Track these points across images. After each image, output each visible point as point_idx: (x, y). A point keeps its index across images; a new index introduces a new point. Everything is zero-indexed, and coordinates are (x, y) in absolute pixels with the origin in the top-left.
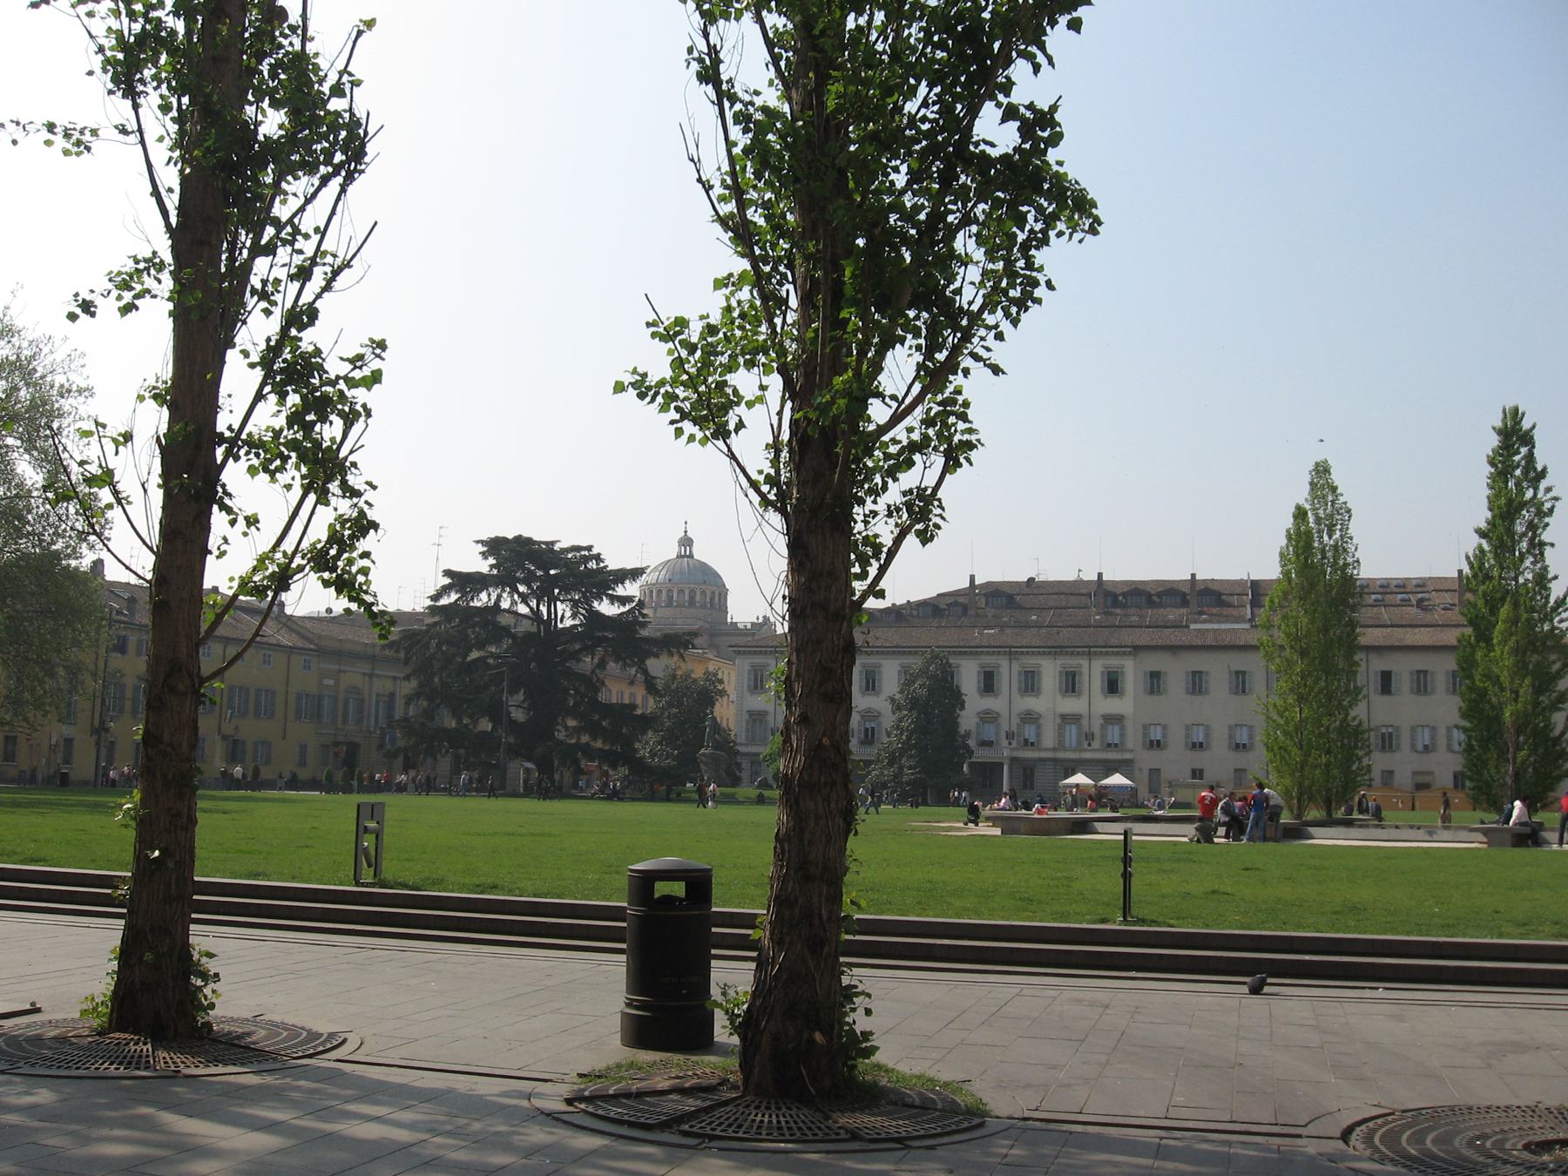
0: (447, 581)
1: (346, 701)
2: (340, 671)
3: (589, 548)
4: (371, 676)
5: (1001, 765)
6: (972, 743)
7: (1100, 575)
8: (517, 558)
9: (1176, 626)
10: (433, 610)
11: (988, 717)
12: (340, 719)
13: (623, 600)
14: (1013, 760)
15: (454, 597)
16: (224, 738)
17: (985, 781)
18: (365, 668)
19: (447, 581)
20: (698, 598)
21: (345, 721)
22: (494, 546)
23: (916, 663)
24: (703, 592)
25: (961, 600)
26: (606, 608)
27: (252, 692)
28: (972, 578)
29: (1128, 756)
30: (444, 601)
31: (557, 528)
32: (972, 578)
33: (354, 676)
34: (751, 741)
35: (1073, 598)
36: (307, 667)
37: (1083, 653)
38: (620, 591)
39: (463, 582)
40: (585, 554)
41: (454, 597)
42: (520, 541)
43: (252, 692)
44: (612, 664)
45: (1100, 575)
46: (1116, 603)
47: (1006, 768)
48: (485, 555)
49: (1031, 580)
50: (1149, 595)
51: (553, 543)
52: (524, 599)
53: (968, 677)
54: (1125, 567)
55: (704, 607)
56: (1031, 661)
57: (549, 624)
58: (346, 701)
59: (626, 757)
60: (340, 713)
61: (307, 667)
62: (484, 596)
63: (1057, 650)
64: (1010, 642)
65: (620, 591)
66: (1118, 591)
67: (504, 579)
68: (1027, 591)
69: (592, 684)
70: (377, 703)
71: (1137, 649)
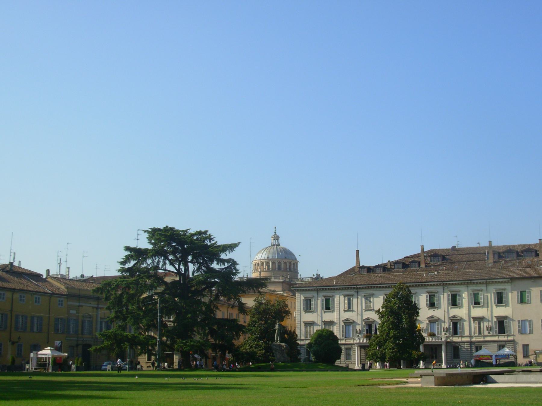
0: (127, 253)
1: (83, 322)
2: (79, 306)
3: (205, 232)
4: (97, 308)
5: (441, 345)
6: (424, 334)
7: (490, 242)
8: (169, 241)
9: (533, 266)
10: (122, 270)
11: (432, 320)
12: (80, 332)
13: (223, 261)
14: (447, 343)
15: (132, 263)
16: (13, 343)
17: (432, 354)
18: (94, 304)
19: (127, 253)
20: (282, 266)
21: (82, 333)
22: (155, 234)
23: (389, 291)
24: (285, 263)
25: (417, 259)
26: (215, 266)
27: (29, 319)
28: (422, 247)
29: (510, 338)
30: (127, 266)
31: (186, 223)
32: (422, 247)
33: (87, 308)
34: (346, 337)
35: (475, 256)
36: (61, 303)
37: (483, 283)
38: (223, 256)
39: (136, 253)
40: (203, 235)
41: (132, 263)
42: (166, 229)
43: (29, 319)
44: (222, 298)
45: (490, 242)
46: (500, 257)
47: (443, 346)
48: (150, 239)
49: (454, 247)
50: (517, 253)
51: (186, 231)
52: (172, 263)
53: (422, 300)
54: (503, 240)
55: (285, 270)
56: (455, 288)
57: (184, 276)
58: (83, 322)
59: (226, 346)
60: (80, 328)
61: (61, 303)
62: (149, 261)
63: (468, 282)
64: (443, 279)
65: (223, 256)
66: (501, 251)
67: (158, 252)
68: (452, 253)
69: (210, 309)
70: (101, 324)
71: (512, 279)
